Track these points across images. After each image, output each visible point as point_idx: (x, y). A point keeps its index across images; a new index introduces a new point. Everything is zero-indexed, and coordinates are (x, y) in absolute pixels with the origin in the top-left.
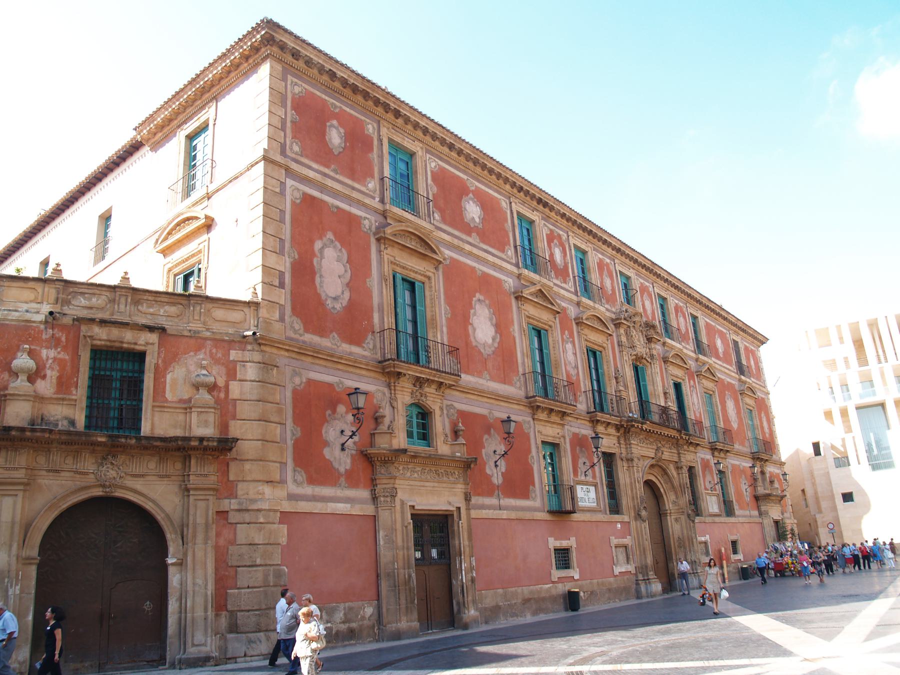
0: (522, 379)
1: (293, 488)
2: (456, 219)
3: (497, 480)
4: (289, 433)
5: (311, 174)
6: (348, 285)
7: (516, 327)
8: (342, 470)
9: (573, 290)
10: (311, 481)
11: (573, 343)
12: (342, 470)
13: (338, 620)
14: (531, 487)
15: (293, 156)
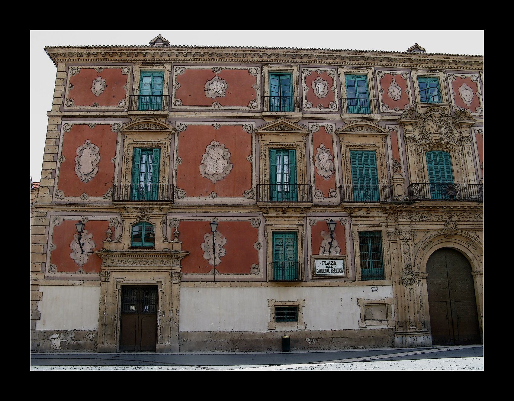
0: (255, 190)
1: (48, 274)
3: (215, 261)
4: (49, 248)
5: (77, 114)
6: (96, 166)
8: (81, 263)
10: (60, 270)
12: (81, 263)
13: (70, 339)
14: (253, 265)
15: (68, 108)
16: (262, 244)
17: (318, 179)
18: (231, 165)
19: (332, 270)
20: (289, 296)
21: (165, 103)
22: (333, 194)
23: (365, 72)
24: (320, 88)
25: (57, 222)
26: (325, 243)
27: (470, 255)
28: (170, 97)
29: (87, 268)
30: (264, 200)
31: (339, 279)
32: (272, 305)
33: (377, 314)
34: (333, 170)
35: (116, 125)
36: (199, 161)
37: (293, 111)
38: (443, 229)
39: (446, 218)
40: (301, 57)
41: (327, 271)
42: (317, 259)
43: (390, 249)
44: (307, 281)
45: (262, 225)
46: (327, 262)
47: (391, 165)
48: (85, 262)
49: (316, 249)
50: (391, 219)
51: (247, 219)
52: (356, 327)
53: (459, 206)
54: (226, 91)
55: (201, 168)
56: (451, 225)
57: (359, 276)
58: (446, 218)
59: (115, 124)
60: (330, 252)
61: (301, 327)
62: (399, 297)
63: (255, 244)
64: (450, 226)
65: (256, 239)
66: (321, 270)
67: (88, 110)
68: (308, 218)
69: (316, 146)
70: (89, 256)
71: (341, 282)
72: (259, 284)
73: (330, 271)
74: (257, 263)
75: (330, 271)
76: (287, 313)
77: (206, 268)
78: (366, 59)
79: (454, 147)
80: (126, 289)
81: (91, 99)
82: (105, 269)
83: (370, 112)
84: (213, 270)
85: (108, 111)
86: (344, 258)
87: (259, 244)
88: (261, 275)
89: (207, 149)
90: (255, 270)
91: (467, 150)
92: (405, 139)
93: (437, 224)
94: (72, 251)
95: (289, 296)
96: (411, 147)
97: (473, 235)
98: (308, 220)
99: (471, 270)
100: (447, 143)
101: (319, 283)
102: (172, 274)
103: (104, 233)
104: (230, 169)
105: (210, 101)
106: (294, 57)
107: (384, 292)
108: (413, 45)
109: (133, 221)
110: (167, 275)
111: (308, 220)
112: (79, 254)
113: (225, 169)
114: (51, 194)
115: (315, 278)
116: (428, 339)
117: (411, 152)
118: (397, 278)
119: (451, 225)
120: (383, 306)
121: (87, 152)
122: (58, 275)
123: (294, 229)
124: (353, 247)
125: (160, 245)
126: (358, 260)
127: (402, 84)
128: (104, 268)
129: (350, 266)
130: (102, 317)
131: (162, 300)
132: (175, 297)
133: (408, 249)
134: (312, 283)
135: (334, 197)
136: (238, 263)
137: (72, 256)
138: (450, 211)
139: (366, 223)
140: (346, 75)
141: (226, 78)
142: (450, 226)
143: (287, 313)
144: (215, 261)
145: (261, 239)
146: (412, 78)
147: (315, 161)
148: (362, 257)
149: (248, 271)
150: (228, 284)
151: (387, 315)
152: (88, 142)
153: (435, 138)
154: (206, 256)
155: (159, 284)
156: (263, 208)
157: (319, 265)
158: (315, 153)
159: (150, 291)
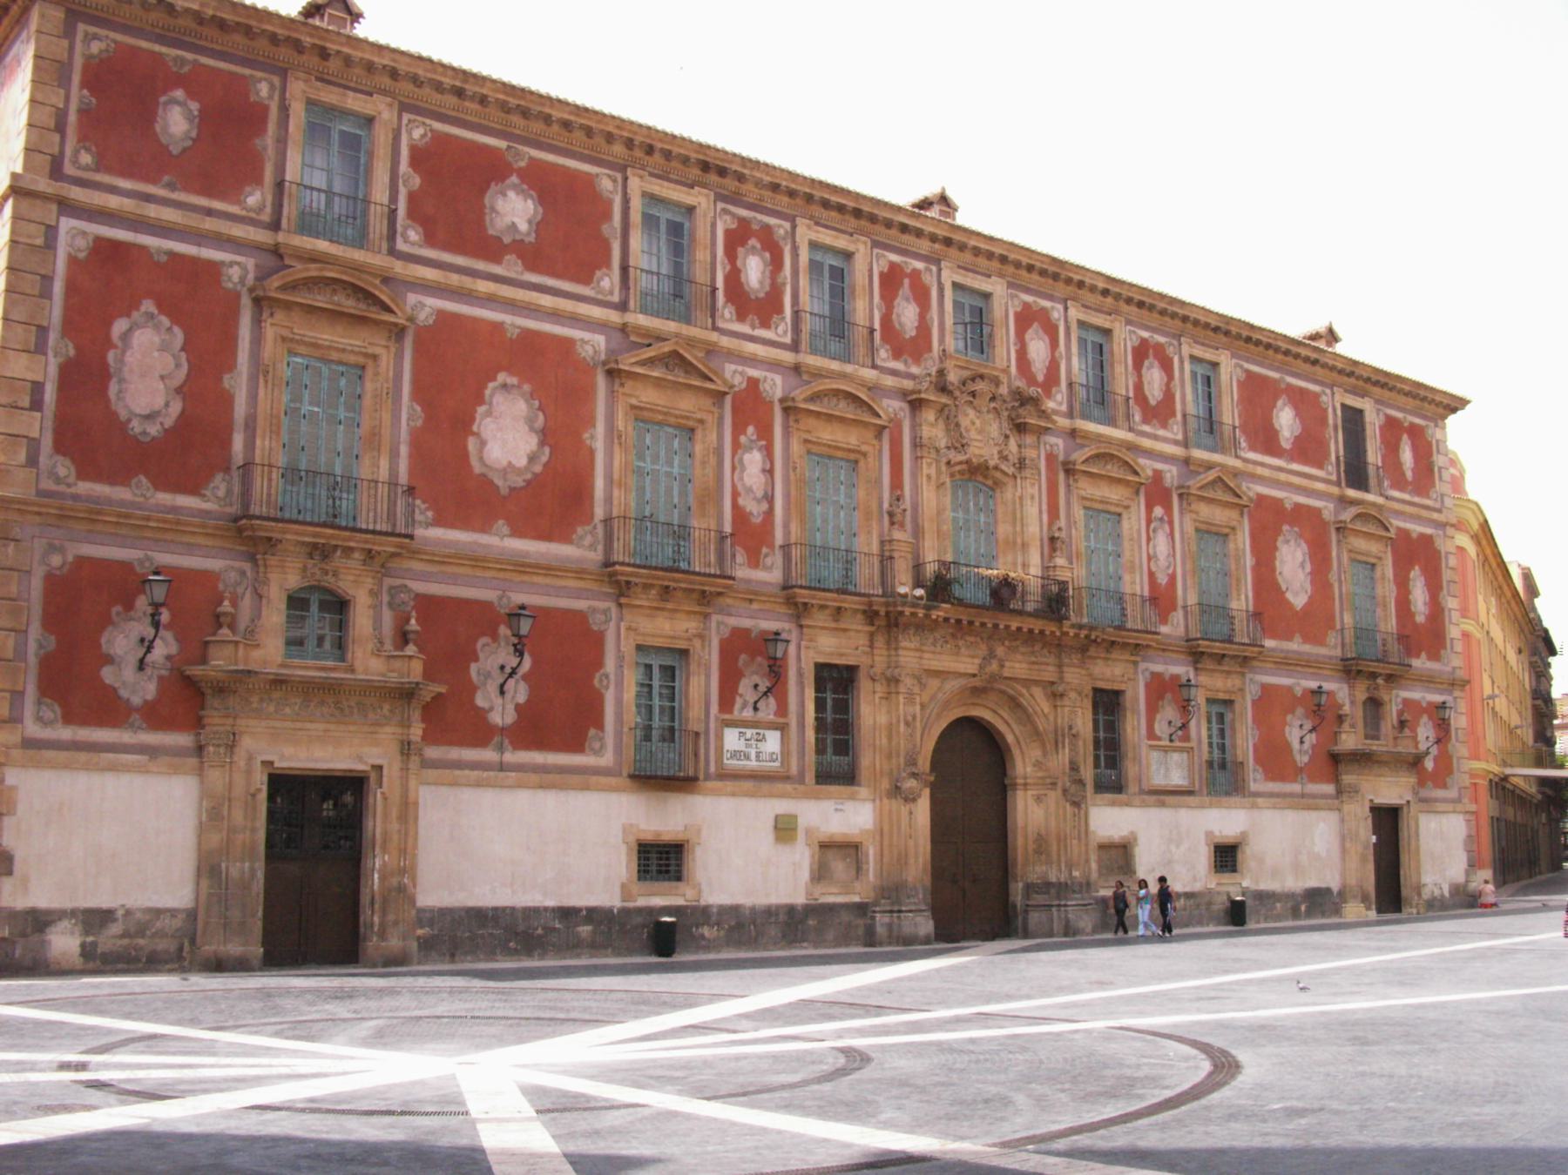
1: (33, 729)
2: (1266, 440)
7: (600, 428)
8: (136, 700)
9: (1334, 478)
10: (69, 718)
11: (768, 452)
12: (136, 700)
16: (612, 677)
17: (740, 515)
18: (547, 450)
19: (758, 754)
20: (665, 818)
21: (378, 226)
22: (769, 561)
23: (851, 248)
24: (754, 270)
25: (56, 560)
26: (745, 687)
27: (1010, 738)
28: (393, 213)
29: (154, 716)
30: (371, 527)
31: (760, 780)
32: (632, 839)
33: (839, 867)
34: (770, 499)
35: (236, 268)
36: (463, 424)
37: (688, 322)
38: (974, 675)
39: (983, 650)
40: (722, 172)
41: (747, 757)
42: (728, 725)
43: (872, 713)
44: (708, 777)
45: (612, 625)
46: (749, 732)
47: (886, 506)
48: (150, 697)
49: (726, 703)
50: (880, 642)
51: (580, 605)
52: (800, 899)
53: (1014, 626)
54: (539, 226)
55: (472, 444)
56: (994, 666)
57: (810, 776)
58: (983, 650)
59: (232, 264)
60: (756, 709)
61: (690, 893)
62: (886, 828)
63: (598, 675)
64: (988, 670)
65: (599, 663)
66: (735, 754)
67: (148, 198)
68: (715, 618)
69: (738, 429)
70: (161, 678)
71: (780, 786)
72: (603, 780)
73: (753, 756)
74: (600, 726)
75: (753, 756)
76: (661, 859)
77: (479, 731)
78: (857, 213)
79: (1005, 479)
80: (284, 785)
81: (148, 160)
82: (1348, 779)
83: (847, 358)
84: (496, 739)
85: (209, 212)
86: (783, 728)
87: (607, 677)
88: (607, 759)
89: (488, 392)
90: (597, 745)
91: (1030, 490)
92: (917, 444)
93: (964, 661)
94: (109, 660)
95: (665, 818)
96: (929, 465)
97: (1024, 691)
98: (714, 625)
99: (1005, 774)
100: (996, 468)
101: (730, 785)
102: (406, 748)
103: (196, 611)
104: (544, 459)
105: (491, 248)
106: (705, 167)
107: (850, 815)
108: (936, 190)
109: (293, 581)
110: (394, 749)
111: (714, 625)
112: (129, 673)
113: (532, 458)
114: (32, 461)
115: (726, 775)
116: (926, 926)
117: (929, 477)
118: (885, 784)
119: (994, 666)
120: (849, 849)
121: (145, 339)
122: (66, 733)
123: (681, 645)
124: (802, 698)
125: (369, 661)
126: (810, 735)
127: (921, 296)
128: (217, 721)
129: (794, 747)
130: (208, 868)
131: (379, 822)
132: (408, 811)
133: (914, 718)
134: (719, 784)
135: (769, 569)
136: (557, 721)
137: (107, 674)
138: (994, 634)
139: (829, 644)
140: (814, 246)
141: (548, 188)
142: (988, 670)
143: (661, 859)
144: (502, 714)
145: (610, 665)
146: (626, 201)
147: (734, 469)
148: (820, 725)
149: (577, 746)
150: (534, 778)
151: (859, 869)
152: (148, 306)
153: (977, 452)
154: (480, 701)
155: (373, 776)
156: (616, 581)
157: (732, 739)
158: (736, 445)
159: (349, 789)
